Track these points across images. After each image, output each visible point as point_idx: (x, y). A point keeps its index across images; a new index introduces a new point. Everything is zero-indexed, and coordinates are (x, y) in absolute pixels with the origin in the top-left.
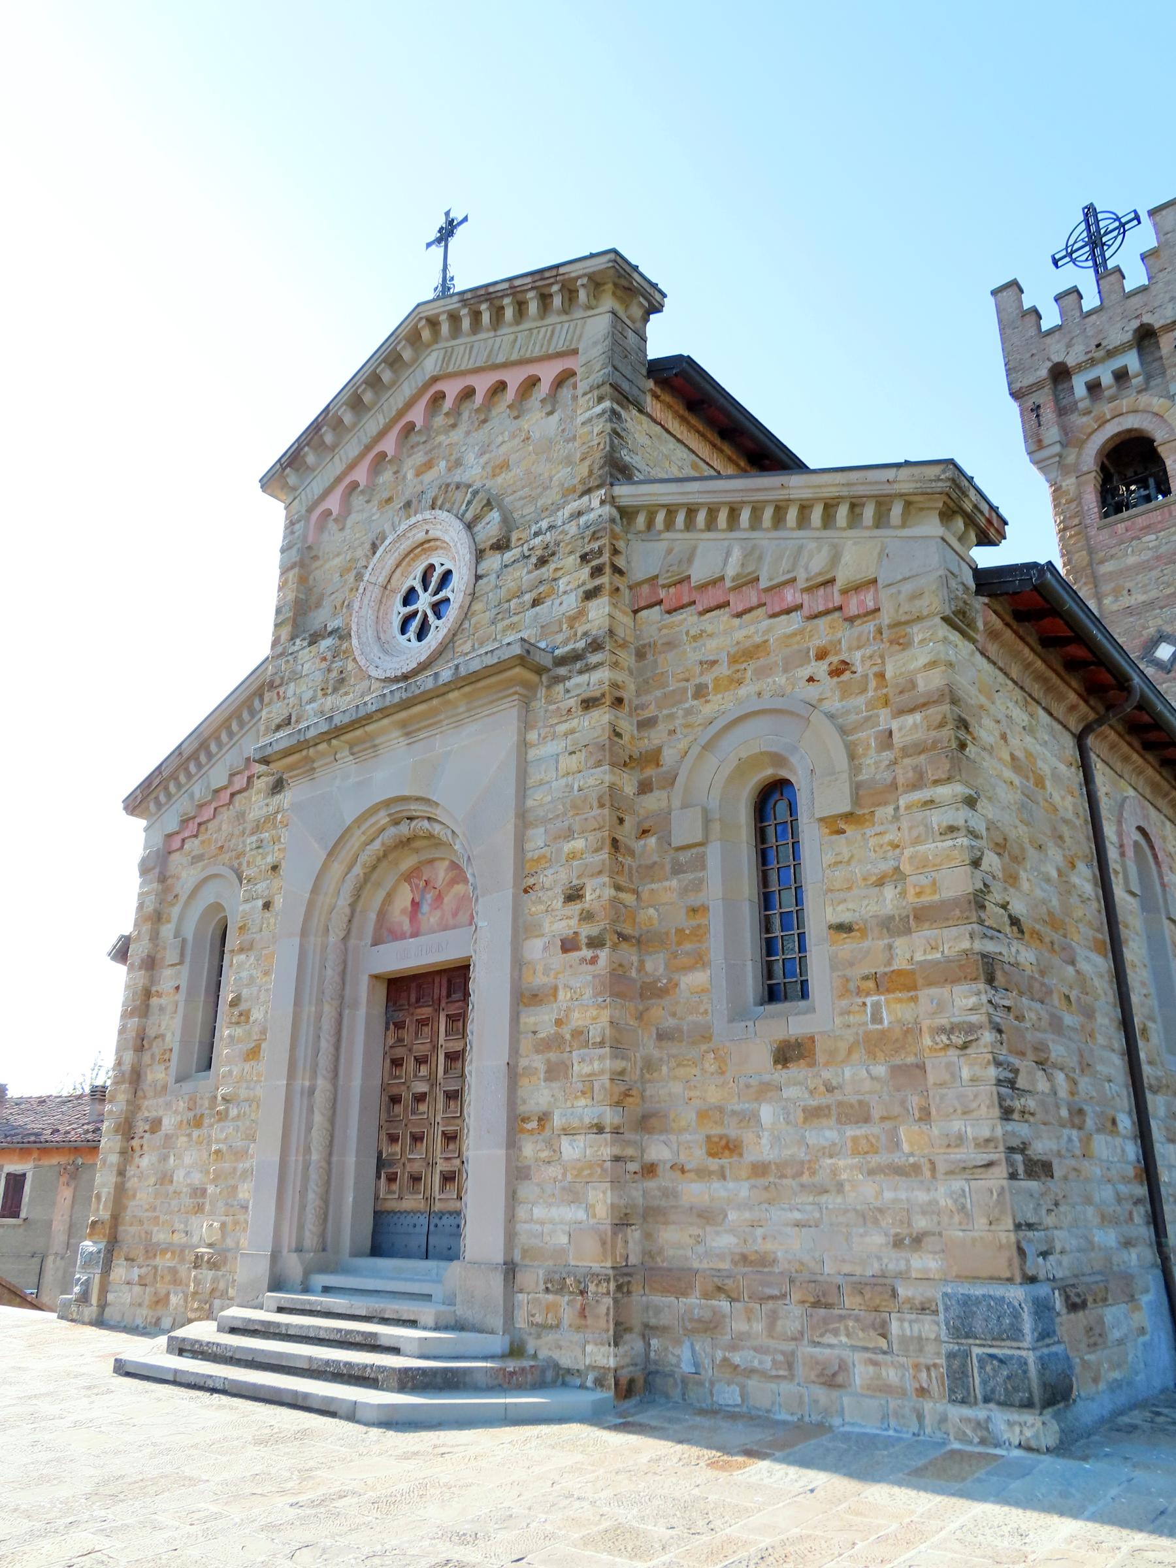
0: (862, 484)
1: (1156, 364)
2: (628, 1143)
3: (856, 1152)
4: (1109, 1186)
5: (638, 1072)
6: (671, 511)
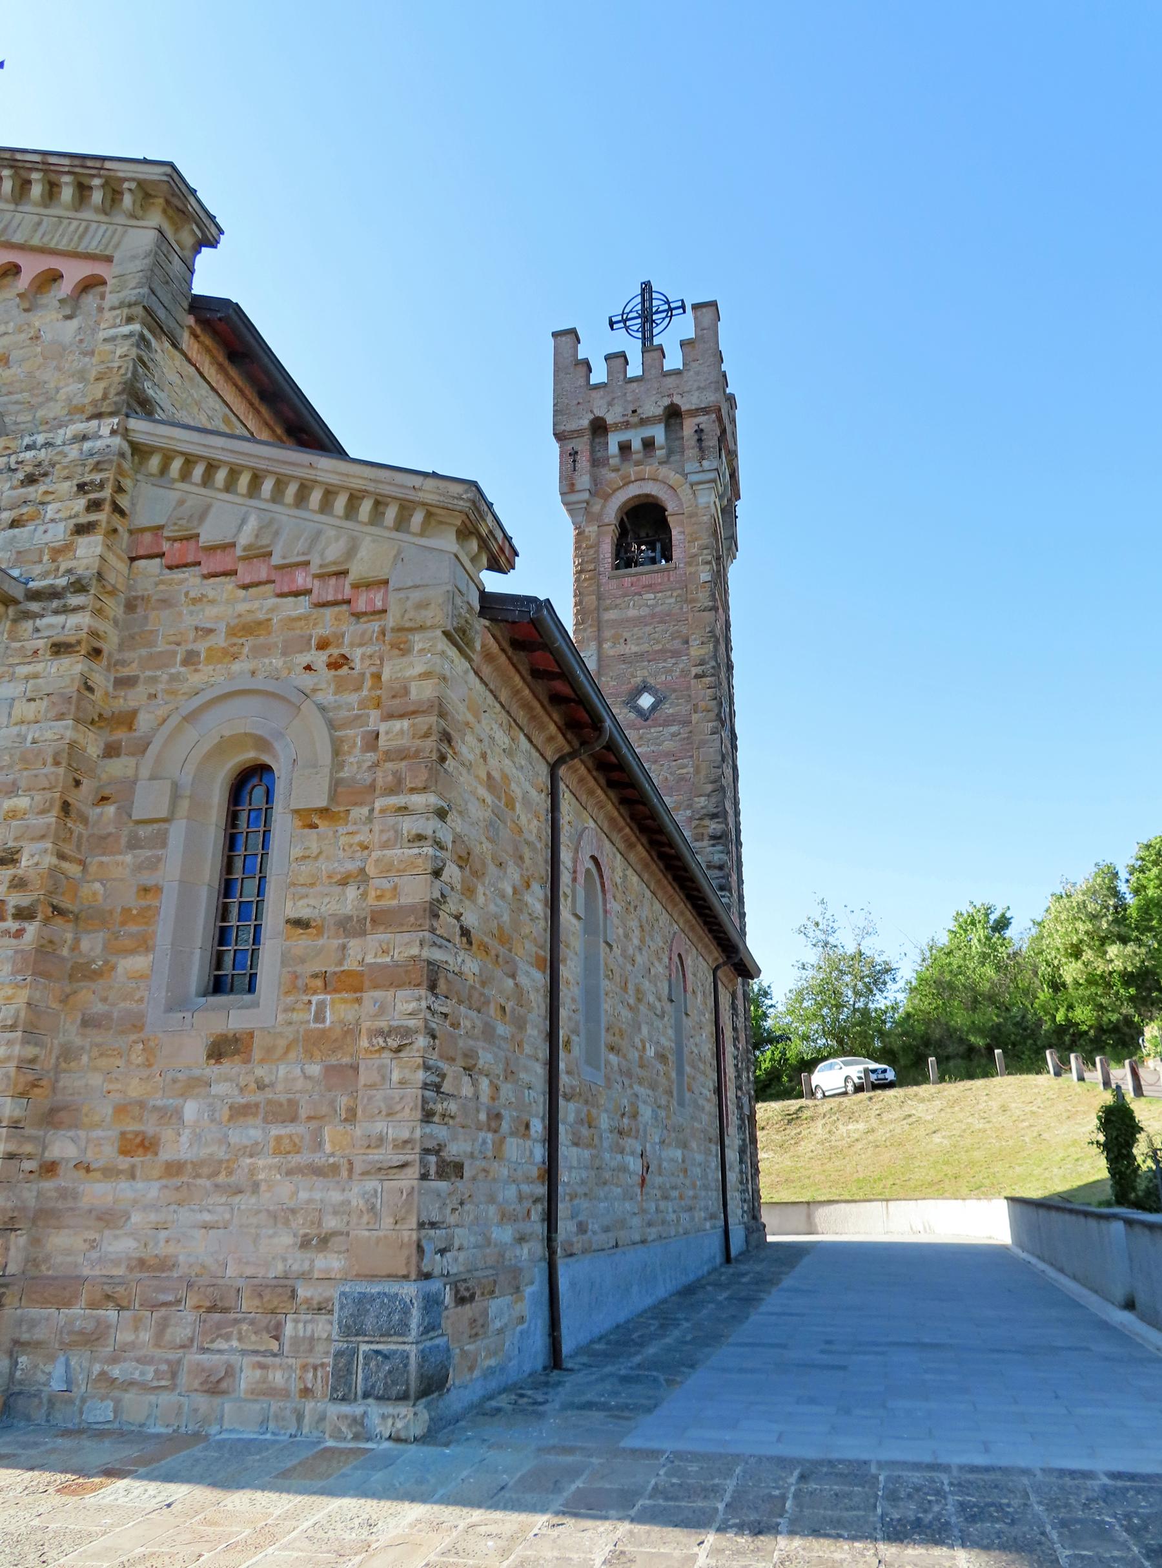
0: (390, 484)
1: (677, 443)
2: (30, 1139)
3: (277, 1152)
4: (514, 1186)
5: (53, 1061)
6: (190, 461)
